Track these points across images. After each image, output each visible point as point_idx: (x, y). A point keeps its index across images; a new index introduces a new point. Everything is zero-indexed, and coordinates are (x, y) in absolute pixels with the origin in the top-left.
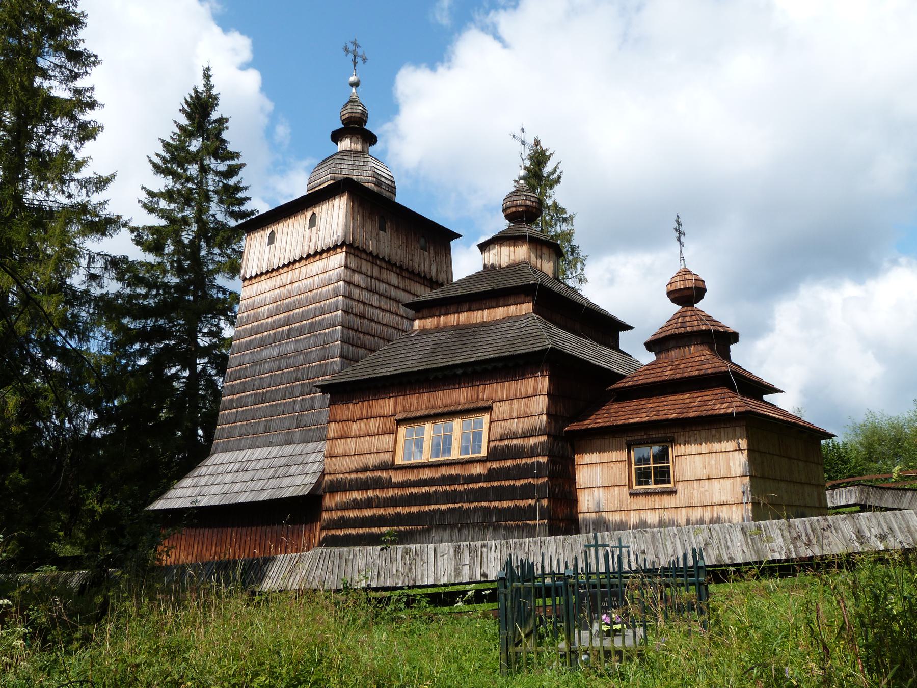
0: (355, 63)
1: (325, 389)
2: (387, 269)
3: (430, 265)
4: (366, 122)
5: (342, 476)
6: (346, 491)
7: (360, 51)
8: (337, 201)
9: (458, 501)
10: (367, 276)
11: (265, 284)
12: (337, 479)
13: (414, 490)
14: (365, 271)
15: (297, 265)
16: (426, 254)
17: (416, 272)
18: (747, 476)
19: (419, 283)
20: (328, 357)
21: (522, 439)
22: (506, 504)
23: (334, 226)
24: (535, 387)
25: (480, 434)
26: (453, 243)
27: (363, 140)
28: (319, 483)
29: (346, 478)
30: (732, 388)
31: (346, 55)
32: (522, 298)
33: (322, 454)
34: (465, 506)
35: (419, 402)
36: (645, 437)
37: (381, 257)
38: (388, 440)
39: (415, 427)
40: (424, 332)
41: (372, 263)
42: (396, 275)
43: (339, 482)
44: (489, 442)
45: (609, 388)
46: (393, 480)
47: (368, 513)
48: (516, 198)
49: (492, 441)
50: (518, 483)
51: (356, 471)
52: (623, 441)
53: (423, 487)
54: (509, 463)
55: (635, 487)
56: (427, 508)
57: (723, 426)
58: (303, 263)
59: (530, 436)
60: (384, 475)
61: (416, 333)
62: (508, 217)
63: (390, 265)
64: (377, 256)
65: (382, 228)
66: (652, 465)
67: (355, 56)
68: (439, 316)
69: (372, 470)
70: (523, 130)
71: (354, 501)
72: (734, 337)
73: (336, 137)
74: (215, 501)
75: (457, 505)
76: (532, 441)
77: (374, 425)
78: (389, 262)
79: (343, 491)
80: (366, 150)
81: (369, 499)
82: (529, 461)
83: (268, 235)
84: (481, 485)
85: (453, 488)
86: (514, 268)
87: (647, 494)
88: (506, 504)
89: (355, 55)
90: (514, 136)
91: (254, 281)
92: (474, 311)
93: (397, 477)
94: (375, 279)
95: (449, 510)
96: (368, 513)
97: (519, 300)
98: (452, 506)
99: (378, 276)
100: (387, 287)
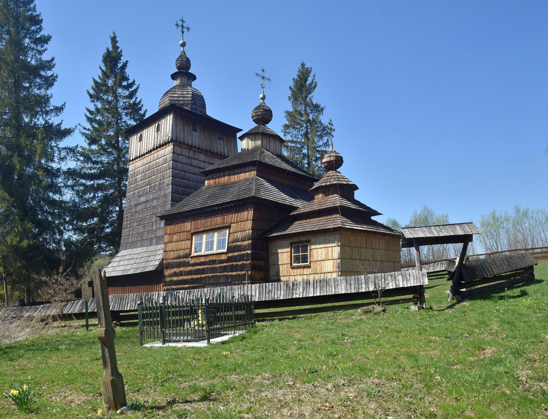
0: (183, 32)
1: (162, 218)
2: (198, 152)
3: (224, 148)
5: (170, 261)
7: (185, 25)
8: (169, 117)
9: (215, 272)
10: (186, 157)
11: (138, 163)
13: (198, 267)
15: (153, 152)
16: (222, 142)
17: (215, 152)
19: (218, 158)
22: (234, 273)
23: (168, 131)
24: (248, 216)
27: (188, 78)
28: (161, 263)
29: (172, 262)
31: (177, 28)
32: (252, 168)
34: (218, 274)
35: (202, 223)
36: (298, 240)
37: (194, 146)
39: (199, 237)
40: (209, 187)
41: (189, 150)
42: (203, 155)
43: (169, 263)
44: (228, 243)
45: (292, 214)
46: (190, 263)
47: (181, 278)
48: (257, 111)
50: (239, 263)
51: (176, 258)
54: (236, 254)
55: (293, 265)
56: (204, 276)
58: (155, 151)
59: (245, 241)
62: (255, 121)
63: (200, 150)
64: (192, 146)
65: (195, 130)
66: (301, 254)
68: (216, 178)
70: (263, 70)
71: (175, 272)
72: (355, 187)
74: (120, 274)
75: (215, 274)
76: (246, 243)
77: (183, 236)
78: (199, 148)
81: (181, 271)
82: (244, 252)
84: (225, 264)
85: (214, 266)
87: (298, 267)
88: (234, 273)
89: (182, 27)
90: (257, 75)
91: (134, 161)
92: (231, 175)
93: (192, 261)
94: (191, 158)
95: (212, 276)
96: (181, 278)
97: (250, 169)
98: (213, 274)
99: (193, 156)
100: (198, 161)
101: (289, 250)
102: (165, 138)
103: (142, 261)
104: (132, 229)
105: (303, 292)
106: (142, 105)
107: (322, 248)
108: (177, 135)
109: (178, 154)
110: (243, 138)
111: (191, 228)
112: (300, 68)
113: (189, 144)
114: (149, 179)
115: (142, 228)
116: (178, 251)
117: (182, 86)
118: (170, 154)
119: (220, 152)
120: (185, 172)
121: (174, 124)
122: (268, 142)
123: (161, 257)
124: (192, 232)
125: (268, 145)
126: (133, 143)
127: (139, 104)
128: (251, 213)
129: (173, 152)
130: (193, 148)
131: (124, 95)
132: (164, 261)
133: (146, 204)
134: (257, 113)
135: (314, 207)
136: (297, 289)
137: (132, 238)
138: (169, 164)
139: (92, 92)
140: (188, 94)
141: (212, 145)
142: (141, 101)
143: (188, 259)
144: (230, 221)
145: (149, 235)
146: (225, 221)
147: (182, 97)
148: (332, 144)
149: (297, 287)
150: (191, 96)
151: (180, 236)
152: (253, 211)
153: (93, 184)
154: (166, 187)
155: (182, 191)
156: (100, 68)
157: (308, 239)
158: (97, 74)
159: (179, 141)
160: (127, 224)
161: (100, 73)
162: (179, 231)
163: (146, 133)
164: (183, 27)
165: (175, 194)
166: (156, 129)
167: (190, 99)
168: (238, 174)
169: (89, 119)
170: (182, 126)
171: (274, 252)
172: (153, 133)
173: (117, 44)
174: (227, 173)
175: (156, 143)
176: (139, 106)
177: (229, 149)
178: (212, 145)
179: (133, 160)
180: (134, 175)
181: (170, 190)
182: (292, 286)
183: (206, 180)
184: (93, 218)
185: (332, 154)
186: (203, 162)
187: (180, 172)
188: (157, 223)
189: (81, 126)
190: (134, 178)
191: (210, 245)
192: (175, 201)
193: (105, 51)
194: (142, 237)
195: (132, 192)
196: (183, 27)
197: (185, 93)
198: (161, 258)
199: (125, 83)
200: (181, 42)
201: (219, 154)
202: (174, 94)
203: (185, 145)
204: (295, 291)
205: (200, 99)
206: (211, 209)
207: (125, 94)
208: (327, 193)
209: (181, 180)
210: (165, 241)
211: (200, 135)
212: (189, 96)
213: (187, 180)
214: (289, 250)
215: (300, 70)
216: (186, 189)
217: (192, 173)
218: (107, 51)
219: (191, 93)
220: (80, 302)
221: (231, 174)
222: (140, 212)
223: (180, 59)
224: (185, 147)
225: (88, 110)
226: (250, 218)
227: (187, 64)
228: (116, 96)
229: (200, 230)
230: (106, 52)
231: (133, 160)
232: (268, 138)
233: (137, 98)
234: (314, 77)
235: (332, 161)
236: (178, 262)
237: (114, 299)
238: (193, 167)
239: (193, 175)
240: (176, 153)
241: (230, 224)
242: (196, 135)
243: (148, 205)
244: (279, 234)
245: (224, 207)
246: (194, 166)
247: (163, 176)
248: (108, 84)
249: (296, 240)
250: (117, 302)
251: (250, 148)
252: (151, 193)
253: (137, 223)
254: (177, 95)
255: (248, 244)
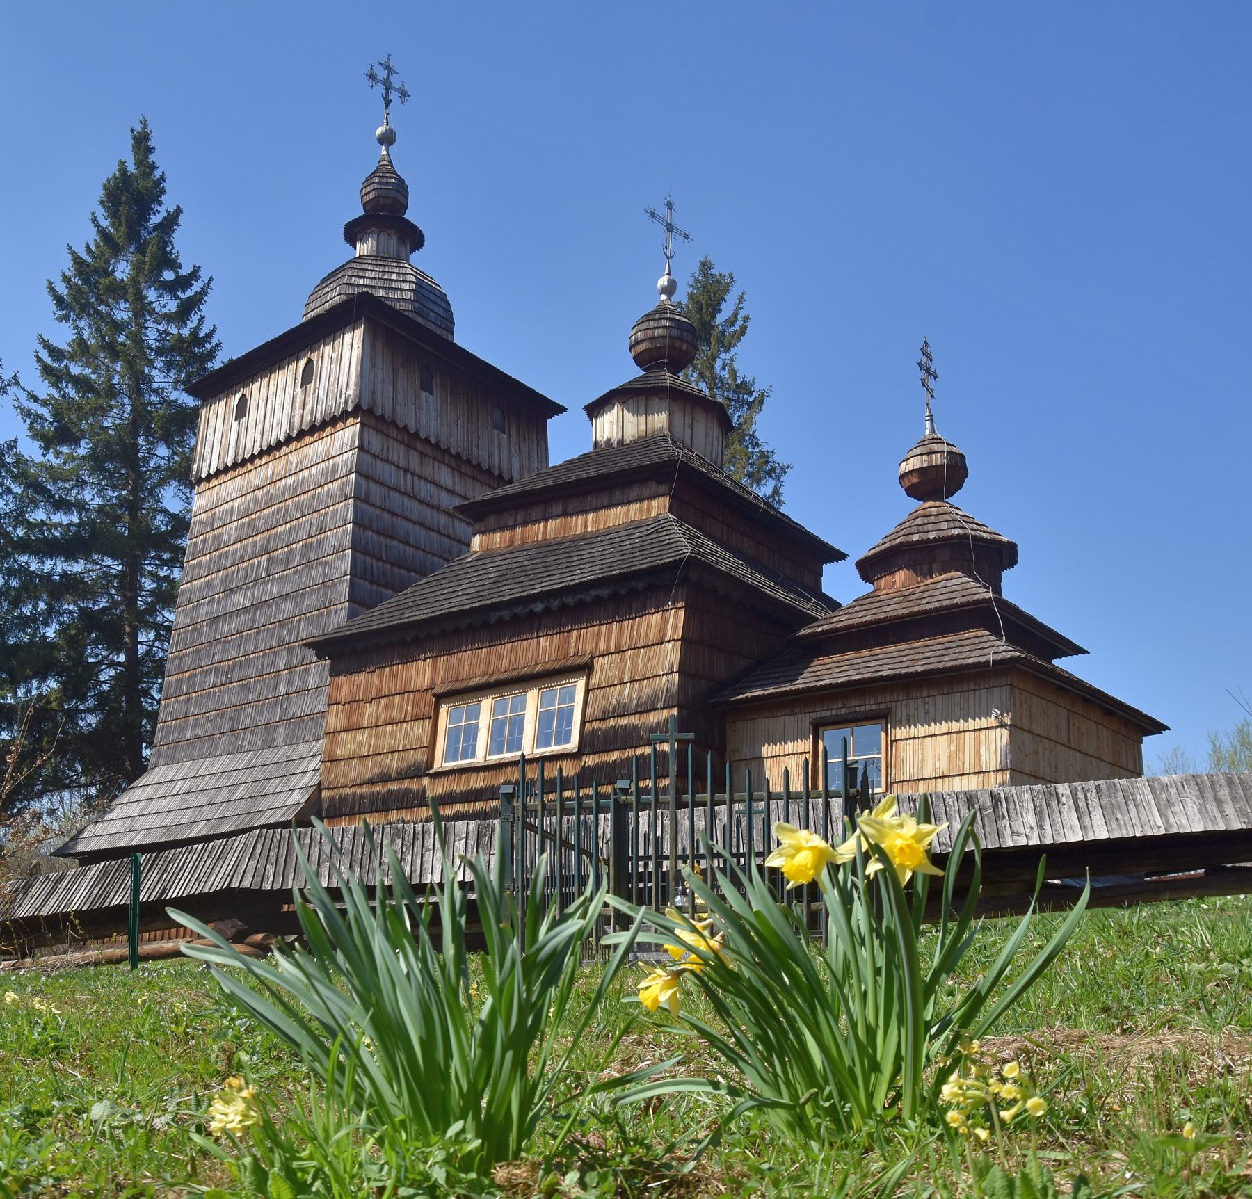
0: (388, 102)
2: (434, 459)
4: (406, 208)
5: (348, 791)
6: (355, 814)
7: (395, 81)
8: (348, 337)
10: (398, 467)
11: (230, 486)
12: (340, 795)
14: (396, 459)
15: (284, 450)
17: (485, 467)
18: (1007, 769)
19: (490, 486)
20: (330, 602)
21: (637, 716)
23: (343, 379)
24: (663, 629)
25: (570, 712)
26: (552, 424)
29: (354, 795)
30: (996, 632)
32: (652, 487)
33: (318, 758)
36: (843, 711)
37: (423, 436)
38: (421, 729)
39: (465, 705)
40: (488, 555)
41: (408, 446)
43: (343, 800)
44: (583, 723)
45: (802, 632)
46: (429, 794)
48: (652, 324)
49: (589, 722)
51: (371, 782)
52: (805, 719)
53: (475, 802)
57: (973, 687)
58: (294, 445)
59: (651, 711)
60: (413, 785)
61: (476, 555)
62: (639, 359)
63: (437, 451)
64: (416, 435)
65: (426, 387)
67: (387, 89)
68: (513, 527)
69: (395, 780)
70: (670, 206)
73: (353, 233)
76: (654, 718)
77: (400, 706)
78: (437, 446)
79: (349, 815)
80: (403, 256)
83: (236, 402)
86: (647, 442)
91: (214, 482)
92: (571, 515)
94: (413, 474)
97: (647, 492)
100: (432, 488)
101: (807, 745)
102: (331, 403)
103: (237, 795)
104: (197, 698)
105: (1041, 827)
106: (218, 345)
107: (936, 735)
108: (373, 393)
109: (375, 456)
110: (603, 407)
111: (433, 678)
112: (697, 275)
113: (409, 428)
114: (266, 534)
115: (235, 692)
116: (378, 759)
117: (380, 258)
118: (350, 453)
119: (500, 467)
120: (393, 514)
121: (367, 359)
122: (688, 419)
123: (310, 779)
124: (438, 690)
125: (688, 431)
126: (212, 424)
127: (207, 341)
128: (676, 619)
129: (361, 448)
130: (419, 446)
131: (164, 311)
132: (324, 794)
133: (255, 615)
134: (650, 333)
135: (888, 608)
136: (1013, 816)
137: (195, 726)
138: (345, 484)
139: (62, 289)
140: (404, 281)
141: (475, 443)
142: (213, 331)
143: (419, 783)
144: (589, 648)
145: (261, 715)
146: (572, 651)
147: (383, 288)
148: (931, 416)
149: (1012, 807)
150: (414, 287)
151: (389, 707)
152: (683, 611)
153: (50, 574)
154: (329, 558)
155: (384, 574)
156: (94, 221)
157: (883, 706)
158: (85, 238)
159: (379, 412)
160: (179, 681)
161: (92, 236)
162: (384, 693)
163: (264, 391)
164: (388, 86)
165: (361, 582)
166: (299, 378)
167: (408, 295)
168: (597, 509)
169: (47, 371)
170: (391, 370)
171: (747, 753)
172: (289, 390)
173: (150, 156)
174: (558, 508)
175: (297, 421)
176: (208, 347)
177: (526, 463)
178: (475, 443)
179: (209, 477)
180: (210, 526)
181: (346, 565)
182: (989, 804)
183: (475, 534)
184: (43, 679)
185: (936, 447)
186: (448, 491)
187: (378, 512)
188: (291, 675)
189: (23, 389)
190: (211, 534)
191: (506, 732)
192: (358, 601)
193: (113, 170)
194: (232, 721)
195: (203, 580)
196: (388, 86)
197: (394, 277)
198: (315, 781)
199: (169, 275)
200: (380, 130)
201: (496, 473)
202: (360, 277)
203: (398, 428)
204: (1006, 822)
205: (438, 301)
206: (519, 610)
207: (164, 306)
208: (925, 567)
209: (382, 539)
210: (331, 727)
211: (442, 406)
212: (407, 286)
213: (400, 541)
214: (807, 745)
215: (697, 281)
216: (396, 569)
217: (414, 523)
218: (120, 170)
219: (413, 279)
220: (90, 874)
221: (570, 510)
222: (229, 641)
223: (376, 180)
224: (395, 435)
225: (46, 345)
226: (673, 633)
227: (400, 198)
228: (142, 309)
229: (470, 684)
230: (114, 174)
231: (209, 477)
232: (688, 411)
233: (203, 318)
234: (740, 302)
235: (938, 468)
236: (378, 793)
237: (259, 846)
238: (417, 504)
239: (417, 528)
240: (368, 452)
241: (592, 658)
242: (430, 401)
243: (261, 616)
244: (772, 690)
245: (570, 600)
246: (421, 502)
247: (322, 522)
248: (113, 271)
249: (834, 712)
250: (273, 858)
251: (628, 438)
252: (274, 579)
253: (216, 677)
254: (367, 282)
255: (666, 721)
